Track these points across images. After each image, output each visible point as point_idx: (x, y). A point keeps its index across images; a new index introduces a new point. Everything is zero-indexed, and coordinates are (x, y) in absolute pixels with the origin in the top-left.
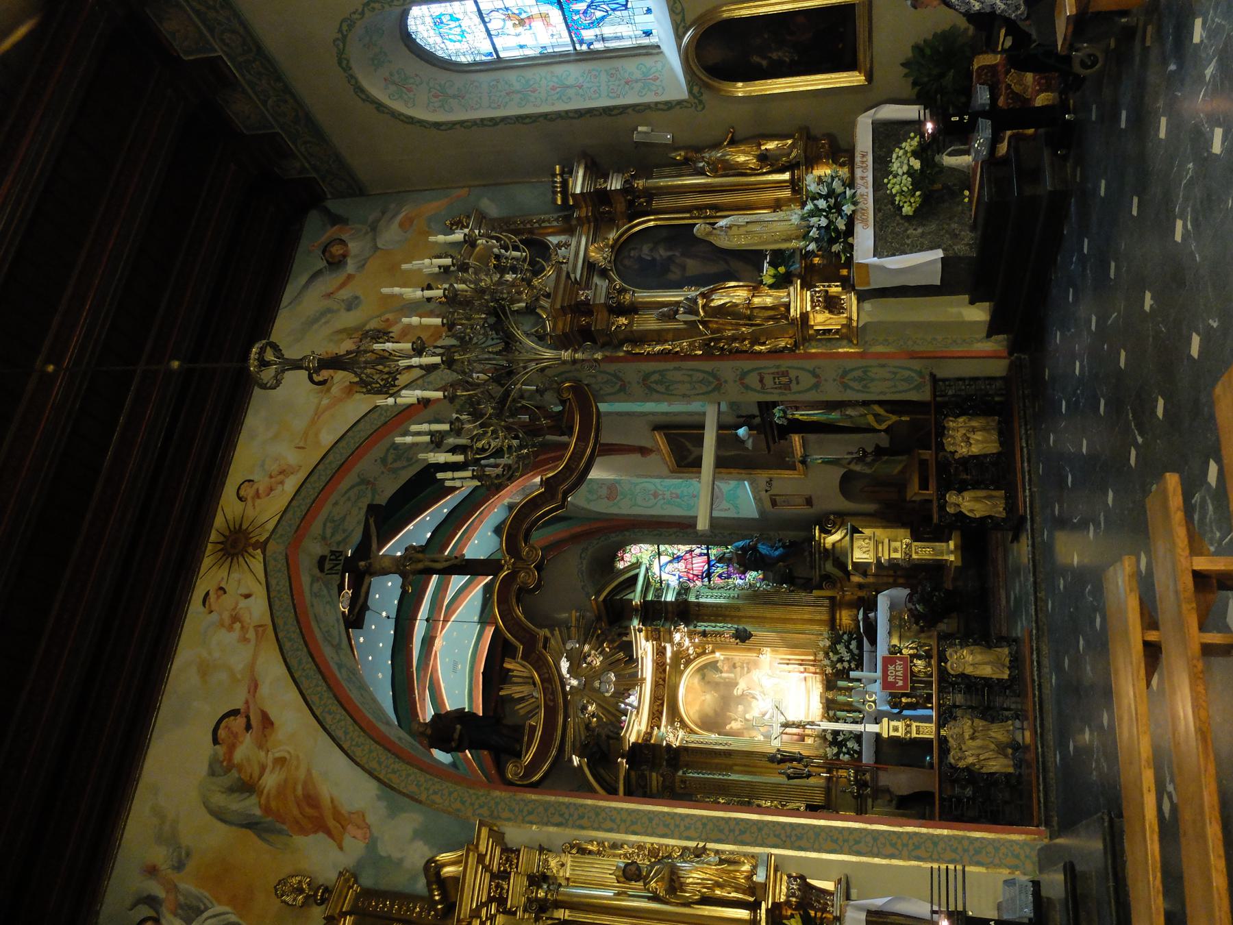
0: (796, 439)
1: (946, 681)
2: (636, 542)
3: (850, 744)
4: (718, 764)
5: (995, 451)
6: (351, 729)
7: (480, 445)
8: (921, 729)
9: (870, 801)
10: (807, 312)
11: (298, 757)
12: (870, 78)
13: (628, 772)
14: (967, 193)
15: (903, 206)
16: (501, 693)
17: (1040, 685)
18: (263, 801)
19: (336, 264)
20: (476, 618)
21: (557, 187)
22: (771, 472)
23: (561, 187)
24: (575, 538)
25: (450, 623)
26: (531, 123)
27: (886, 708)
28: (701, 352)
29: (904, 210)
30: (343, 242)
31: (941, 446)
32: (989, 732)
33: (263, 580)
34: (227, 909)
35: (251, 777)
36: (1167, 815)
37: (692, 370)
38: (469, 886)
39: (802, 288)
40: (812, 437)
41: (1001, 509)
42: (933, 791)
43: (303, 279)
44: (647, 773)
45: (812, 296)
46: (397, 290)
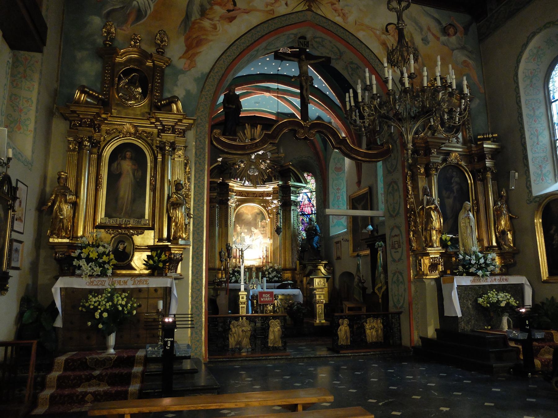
0: (368, 252)
1: (266, 320)
2: (316, 181)
3: (234, 278)
4: (222, 221)
5: (367, 340)
6: (231, 58)
7: (366, 108)
8: (243, 309)
9: (213, 287)
10: (430, 255)
12: (545, 282)
13: (216, 183)
14: (489, 327)
15: (482, 298)
17: (266, 359)
18: (198, 21)
19: (445, 31)
21: (486, 135)
22: (352, 241)
23: (486, 137)
24: (317, 154)
25: (277, 99)
26: (518, 120)
27: (251, 294)
28: (408, 207)
29: (480, 299)
30: (455, 33)
31: (368, 316)
32: (245, 338)
33: (294, 11)
34: (152, 10)
36: (221, 412)
37: (400, 203)
38: (169, 116)
39: (441, 253)
40: (369, 259)
41: (342, 343)
42: (219, 313)
43: (436, 16)
44: (216, 191)
45: (437, 257)
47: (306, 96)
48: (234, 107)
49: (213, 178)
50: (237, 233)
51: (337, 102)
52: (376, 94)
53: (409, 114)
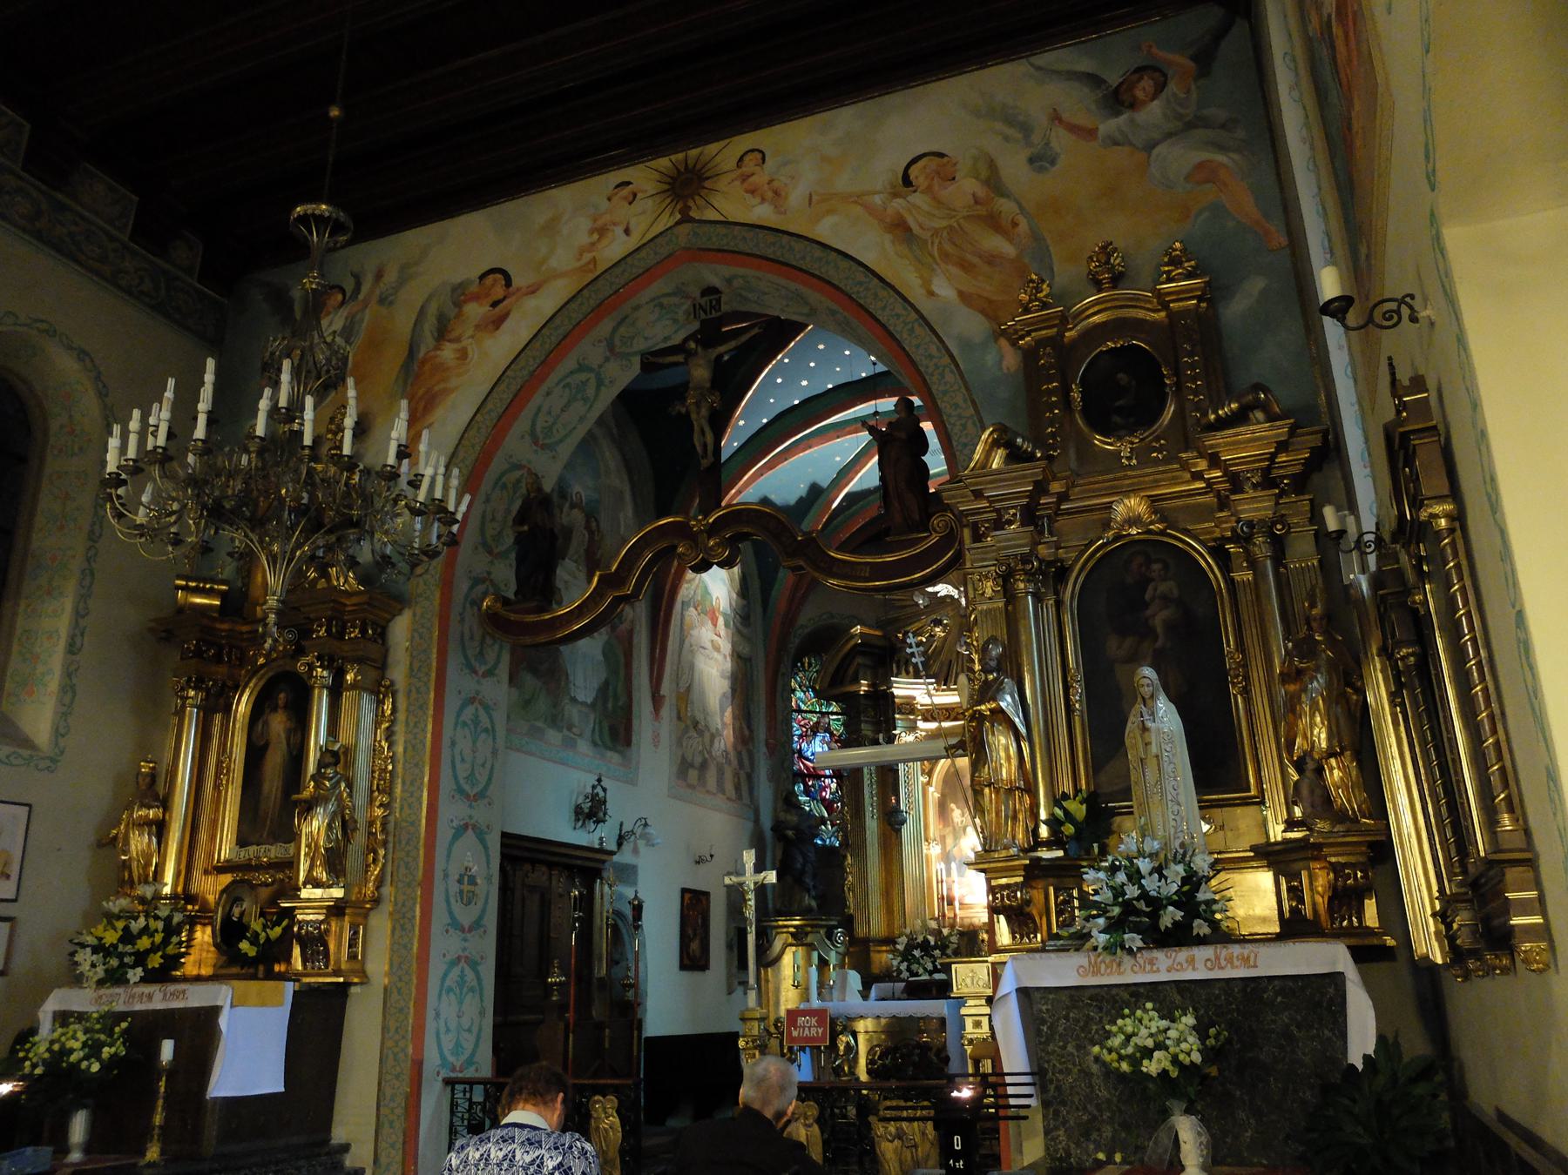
18: (432, 353)
30: (1160, 88)
50: (954, 829)
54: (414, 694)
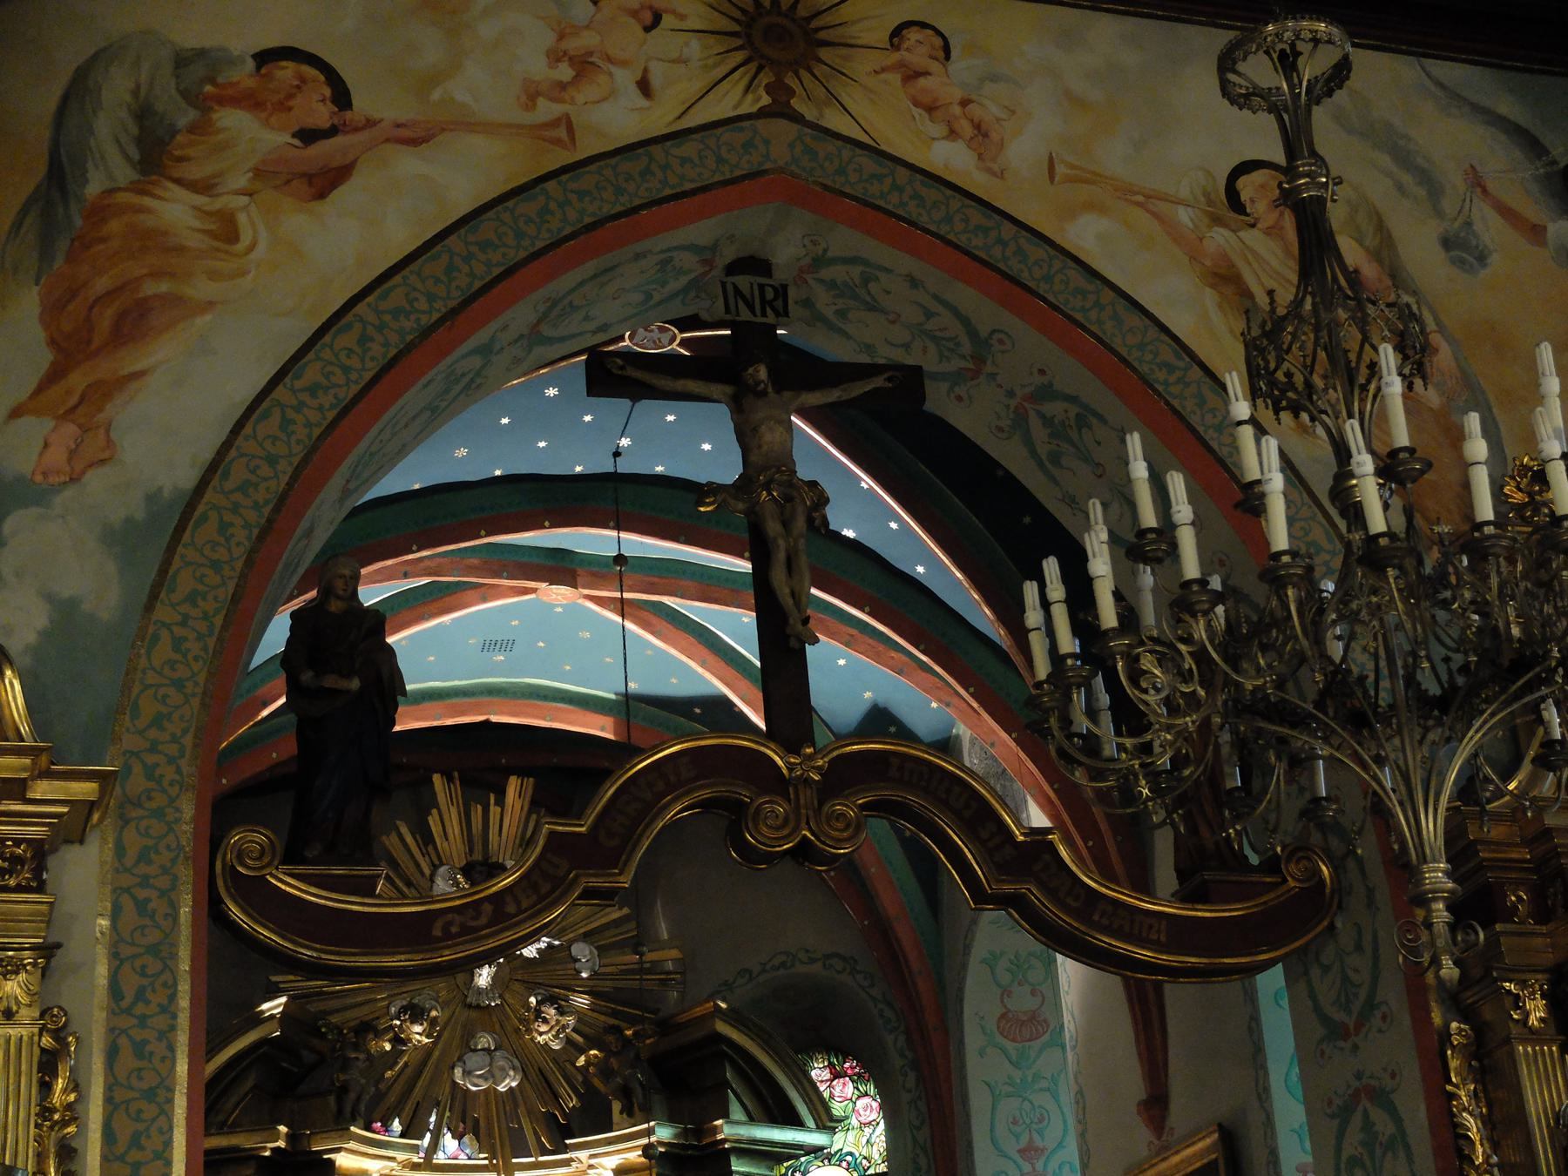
2: (890, 1110)
7: (1148, 662)
11: (243, 273)
13: (251, 1157)
16: (437, 778)
20: (633, 686)
24: (881, 932)
25: (619, 619)
35: (180, 159)
43: (1507, 107)
46: (1553, 385)
47: (787, 602)
48: (355, 684)
49: (234, 1128)
51: (983, 617)
52: (1203, 582)
53: (1410, 680)
54: (127, 1060)
